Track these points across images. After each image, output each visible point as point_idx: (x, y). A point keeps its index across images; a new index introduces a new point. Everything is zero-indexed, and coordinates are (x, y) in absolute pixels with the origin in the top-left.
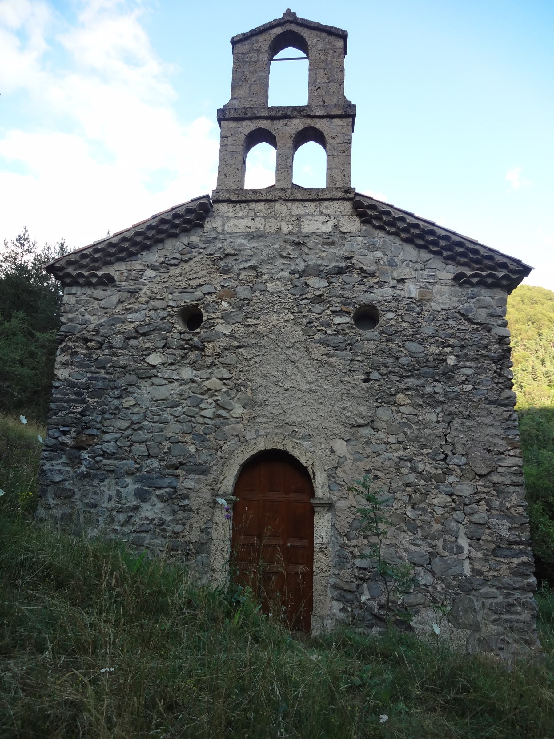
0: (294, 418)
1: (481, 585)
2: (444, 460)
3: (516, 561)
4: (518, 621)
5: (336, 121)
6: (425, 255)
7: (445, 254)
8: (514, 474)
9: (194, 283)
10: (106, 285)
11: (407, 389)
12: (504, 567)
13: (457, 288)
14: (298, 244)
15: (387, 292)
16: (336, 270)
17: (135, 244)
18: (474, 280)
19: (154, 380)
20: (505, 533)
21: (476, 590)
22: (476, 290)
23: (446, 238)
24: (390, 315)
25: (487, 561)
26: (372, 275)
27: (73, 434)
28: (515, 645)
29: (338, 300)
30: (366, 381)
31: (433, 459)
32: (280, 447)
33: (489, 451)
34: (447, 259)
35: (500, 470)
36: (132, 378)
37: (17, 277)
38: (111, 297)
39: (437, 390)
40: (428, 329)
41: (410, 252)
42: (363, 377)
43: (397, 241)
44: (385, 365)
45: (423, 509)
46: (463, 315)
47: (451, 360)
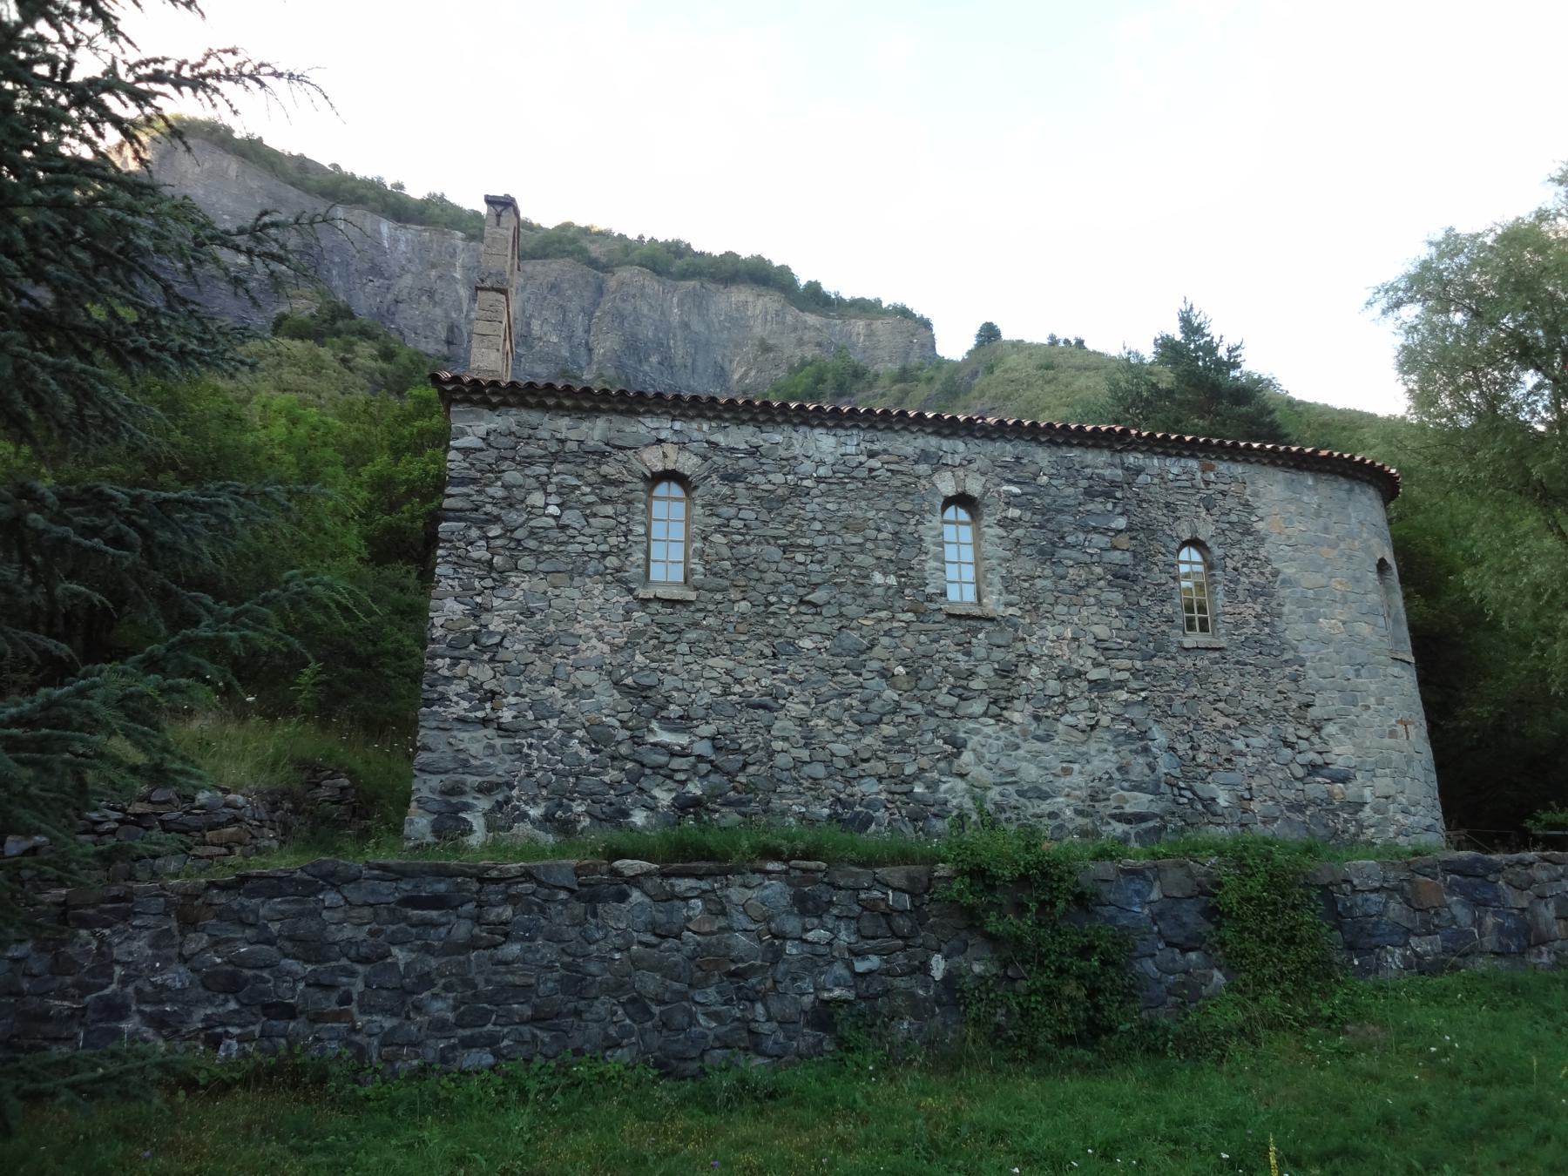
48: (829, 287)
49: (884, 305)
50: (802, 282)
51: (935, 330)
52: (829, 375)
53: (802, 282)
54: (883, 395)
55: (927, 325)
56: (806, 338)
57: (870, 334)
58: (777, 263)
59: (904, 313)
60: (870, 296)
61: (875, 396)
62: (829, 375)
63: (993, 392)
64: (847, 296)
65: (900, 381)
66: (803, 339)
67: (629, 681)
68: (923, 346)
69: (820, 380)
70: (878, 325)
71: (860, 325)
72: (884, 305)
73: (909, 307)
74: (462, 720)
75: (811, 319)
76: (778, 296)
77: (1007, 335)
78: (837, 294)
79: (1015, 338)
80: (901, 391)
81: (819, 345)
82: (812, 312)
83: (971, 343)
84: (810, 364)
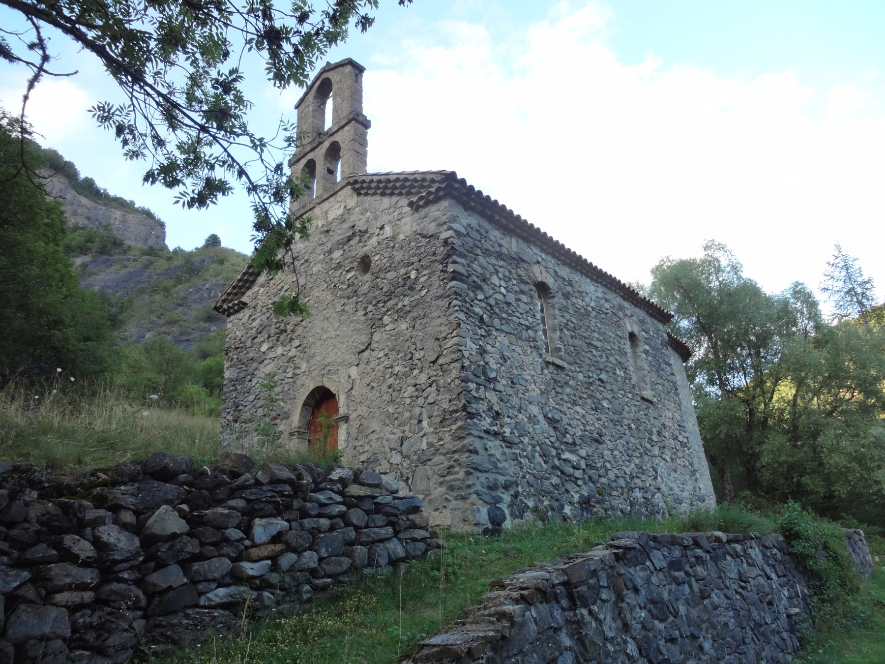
0: (329, 360)
1: (433, 454)
2: (411, 359)
3: (454, 427)
4: (454, 480)
5: (347, 128)
6: (395, 199)
7: (379, 192)
8: (454, 353)
9: (279, 287)
10: (243, 308)
11: (388, 311)
12: (447, 434)
13: (416, 215)
14: (328, 231)
15: (374, 241)
16: (346, 240)
17: (251, 274)
18: (421, 203)
19: (266, 362)
20: (446, 405)
21: (429, 460)
22: (426, 210)
23: (397, 180)
24: (377, 257)
25: (437, 433)
26: (366, 232)
27: (232, 413)
28: (455, 502)
29: (347, 261)
30: (365, 315)
31: (405, 360)
32: (320, 384)
33: (438, 339)
34: (383, 194)
35: (445, 352)
36: (255, 365)
37: (671, 346)
38: (244, 315)
39: (405, 303)
40: (399, 256)
41: (386, 201)
42: (362, 313)
43: (378, 197)
44: (375, 298)
45: (399, 404)
46: (420, 234)
47: (413, 275)
48: (101, 184)
49: (137, 206)
50: (82, 176)
51: (167, 230)
52: (98, 239)
53: (82, 176)
54: (135, 260)
55: (162, 225)
56: (79, 211)
57: (123, 221)
58: (67, 158)
59: (148, 214)
60: (128, 198)
61: (128, 260)
62: (98, 239)
63: (224, 275)
64: (112, 193)
65: (148, 254)
66: (395, 177)
67: (550, 415)
68: (158, 237)
69: (90, 240)
70: (130, 217)
71: (118, 214)
72: (137, 206)
73: (152, 211)
74: (487, 432)
75: (84, 201)
76: (63, 180)
77: (224, 244)
78: (105, 190)
79: (230, 247)
80: (148, 261)
81: (88, 218)
82: (86, 196)
83: (201, 243)
84: (82, 229)
